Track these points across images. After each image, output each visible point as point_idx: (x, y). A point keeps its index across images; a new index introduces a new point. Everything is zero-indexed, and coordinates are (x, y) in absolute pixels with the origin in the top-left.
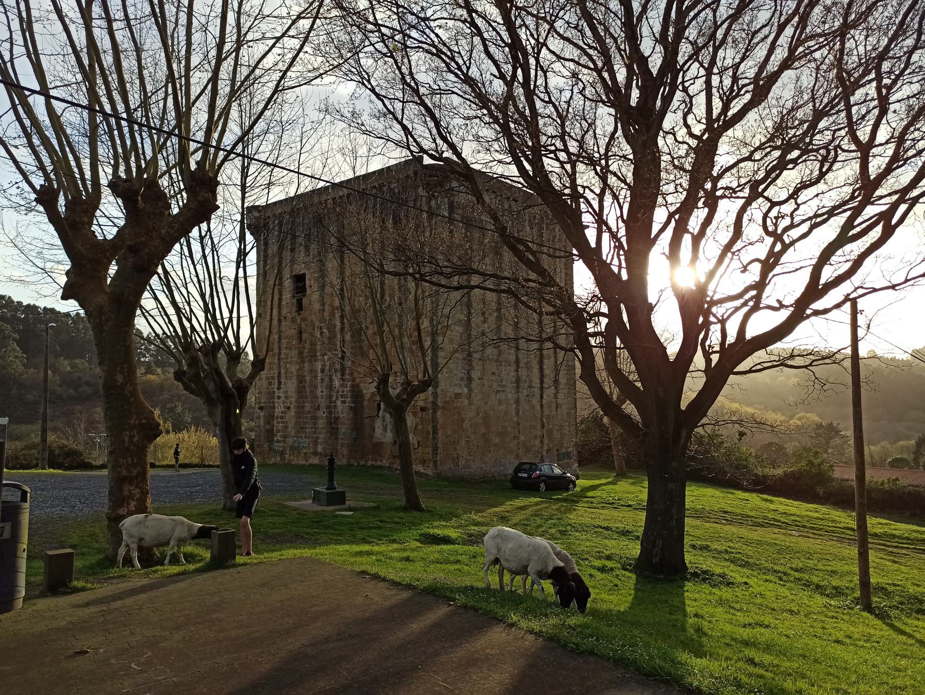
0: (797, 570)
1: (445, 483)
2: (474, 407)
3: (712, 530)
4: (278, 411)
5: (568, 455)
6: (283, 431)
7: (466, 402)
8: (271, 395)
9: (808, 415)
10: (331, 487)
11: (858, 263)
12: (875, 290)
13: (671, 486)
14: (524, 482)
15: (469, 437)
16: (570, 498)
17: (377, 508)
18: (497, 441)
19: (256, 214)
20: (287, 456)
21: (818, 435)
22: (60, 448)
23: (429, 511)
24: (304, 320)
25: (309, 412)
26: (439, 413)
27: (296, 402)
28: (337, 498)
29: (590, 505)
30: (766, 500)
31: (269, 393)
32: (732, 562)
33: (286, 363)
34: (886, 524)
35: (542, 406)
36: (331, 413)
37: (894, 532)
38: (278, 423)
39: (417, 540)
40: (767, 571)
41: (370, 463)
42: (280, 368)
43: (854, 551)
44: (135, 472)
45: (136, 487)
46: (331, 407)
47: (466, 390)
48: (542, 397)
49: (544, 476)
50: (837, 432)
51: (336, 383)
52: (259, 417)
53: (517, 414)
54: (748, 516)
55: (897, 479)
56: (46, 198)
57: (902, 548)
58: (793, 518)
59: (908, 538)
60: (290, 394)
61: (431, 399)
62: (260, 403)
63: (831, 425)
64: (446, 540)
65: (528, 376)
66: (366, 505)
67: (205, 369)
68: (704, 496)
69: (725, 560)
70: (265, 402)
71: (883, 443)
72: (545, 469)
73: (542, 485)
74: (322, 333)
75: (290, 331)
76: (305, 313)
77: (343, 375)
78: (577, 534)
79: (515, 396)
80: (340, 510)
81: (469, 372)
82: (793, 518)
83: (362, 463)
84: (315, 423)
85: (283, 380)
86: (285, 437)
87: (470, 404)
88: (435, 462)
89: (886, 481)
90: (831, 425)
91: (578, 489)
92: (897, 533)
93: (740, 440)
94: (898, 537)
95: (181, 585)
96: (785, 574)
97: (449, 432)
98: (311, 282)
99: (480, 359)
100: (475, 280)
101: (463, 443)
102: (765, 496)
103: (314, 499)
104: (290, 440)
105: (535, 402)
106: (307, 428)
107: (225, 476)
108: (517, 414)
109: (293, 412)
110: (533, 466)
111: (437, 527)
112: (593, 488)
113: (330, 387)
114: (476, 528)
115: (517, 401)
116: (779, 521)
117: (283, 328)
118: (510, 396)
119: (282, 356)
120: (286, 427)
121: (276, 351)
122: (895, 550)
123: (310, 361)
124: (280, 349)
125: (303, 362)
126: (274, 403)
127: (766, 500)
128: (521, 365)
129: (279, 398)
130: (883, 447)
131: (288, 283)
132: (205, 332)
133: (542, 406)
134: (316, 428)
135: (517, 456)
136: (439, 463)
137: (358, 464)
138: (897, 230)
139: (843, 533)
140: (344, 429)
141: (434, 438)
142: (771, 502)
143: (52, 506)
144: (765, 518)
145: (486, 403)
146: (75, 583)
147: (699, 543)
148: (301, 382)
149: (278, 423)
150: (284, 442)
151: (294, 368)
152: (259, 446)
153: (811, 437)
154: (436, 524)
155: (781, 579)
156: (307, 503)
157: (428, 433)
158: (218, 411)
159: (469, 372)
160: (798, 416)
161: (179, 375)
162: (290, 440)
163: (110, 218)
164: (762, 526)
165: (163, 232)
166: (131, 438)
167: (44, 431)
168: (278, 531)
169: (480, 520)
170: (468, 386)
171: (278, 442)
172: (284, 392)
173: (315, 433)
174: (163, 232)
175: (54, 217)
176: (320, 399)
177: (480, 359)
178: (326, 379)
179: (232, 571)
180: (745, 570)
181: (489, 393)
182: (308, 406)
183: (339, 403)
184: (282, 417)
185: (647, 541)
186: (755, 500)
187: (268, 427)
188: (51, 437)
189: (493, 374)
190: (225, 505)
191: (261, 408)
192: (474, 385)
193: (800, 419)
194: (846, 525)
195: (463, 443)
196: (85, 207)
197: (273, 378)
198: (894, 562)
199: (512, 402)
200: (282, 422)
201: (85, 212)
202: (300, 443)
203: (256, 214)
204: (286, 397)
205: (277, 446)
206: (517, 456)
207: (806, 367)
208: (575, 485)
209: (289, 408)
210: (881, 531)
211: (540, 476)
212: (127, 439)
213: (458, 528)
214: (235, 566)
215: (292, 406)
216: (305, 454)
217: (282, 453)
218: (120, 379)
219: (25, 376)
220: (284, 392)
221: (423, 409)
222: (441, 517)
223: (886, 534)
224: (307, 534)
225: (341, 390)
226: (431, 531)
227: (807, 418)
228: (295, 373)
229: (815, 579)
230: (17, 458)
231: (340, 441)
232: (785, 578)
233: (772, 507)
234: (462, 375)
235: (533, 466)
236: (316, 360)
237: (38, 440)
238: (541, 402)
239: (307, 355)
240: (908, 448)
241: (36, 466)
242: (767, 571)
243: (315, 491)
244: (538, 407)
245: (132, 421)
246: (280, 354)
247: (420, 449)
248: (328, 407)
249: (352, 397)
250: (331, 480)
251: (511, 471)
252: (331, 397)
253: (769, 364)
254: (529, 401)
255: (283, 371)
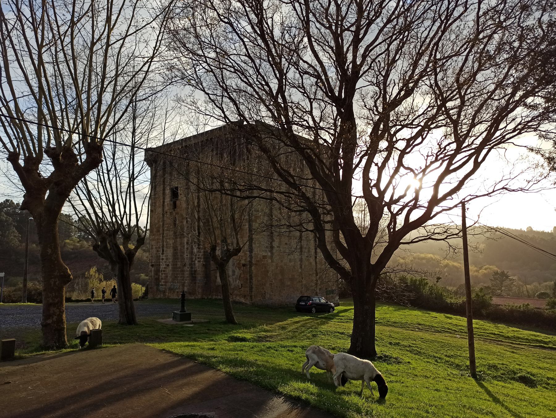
0: (449, 357)
2: (274, 264)
3: (406, 334)
4: (162, 267)
5: (332, 292)
7: (270, 261)
8: (158, 258)
9: (491, 267)
10: (183, 310)
11: (461, 183)
12: (477, 197)
13: (366, 307)
14: (303, 307)
17: (209, 322)
18: (289, 283)
20: (167, 294)
21: (496, 279)
22: (35, 290)
24: (177, 213)
25: (180, 268)
26: (253, 268)
27: (172, 262)
28: (185, 317)
30: (448, 317)
32: (411, 352)
33: (167, 239)
34: (517, 331)
35: (316, 262)
36: (192, 268)
37: (519, 336)
38: (162, 274)
41: (214, 297)
43: (466, 342)
44: (56, 301)
46: (192, 264)
47: (269, 254)
48: (316, 257)
50: (507, 277)
51: (195, 250)
53: (301, 267)
54: (433, 327)
55: (528, 305)
56: (13, 158)
57: (522, 345)
58: (460, 327)
59: (527, 339)
60: (169, 257)
61: (248, 259)
62: (152, 262)
64: (243, 340)
65: (307, 245)
67: (111, 242)
68: (410, 315)
69: (407, 350)
71: (534, 284)
72: (316, 300)
73: (314, 309)
74: (187, 222)
75: (168, 220)
76: (178, 210)
77: (199, 245)
78: (323, 336)
79: (300, 257)
80: (186, 324)
81: (271, 243)
82: (460, 327)
83: (210, 297)
84: (183, 274)
85: (165, 249)
86: (166, 282)
87: (272, 262)
88: (251, 296)
91: (335, 312)
92: (521, 336)
93: (437, 282)
94: (521, 338)
96: (440, 358)
97: (259, 279)
102: (448, 315)
103: (173, 318)
104: (169, 284)
105: (312, 260)
107: (120, 304)
108: (301, 267)
109: (170, 268)
110: (309, 298)
111: (240, 333)
112: (345, 311)
113: (192, 253)
114: (264, 333)
115: (301, 260)
116: (451, 329)
117: (165, 219)
118: (296, 257)
119: (165, 235)
120: (167, 277)
122: (516, 346)
123: (180, 238)
124: (163, 230)
125: (176, 238)
126: (160, 262)
127: (448, 317)
128: (303, 238)
129: (163, 259)
130: (535, 286)
131: (168, 191)
132: (122, 219)
133: (316, 262)
134: (184, 277)
135: (301, 292)
137: (208, 298)
138: (482, 165)
139: (488, 336)
141: (250, 282)
142: (451, 318)
143: (24, 323)
145: (282, 261)
146: (16, 354)
147: (394, 341)
149: (162, 274)
150: (166, 285)
151: (171, 242)
152: (151, 288)
153: (492, 280)
154: (241, 331)
155: (436, 361)
156: (170, 321)
157: (247, 279)
158: (117, 268)
159: (271, 243)
160: (485, 267)
161: (95, 247)
162: (169, 284)
164: (440, 332)
165: (73, 174)
166: (55, 282)
167: (25, 280)
168: (147, 335)
169: (269, 329)
171: (162, 285)
172: (166, 256)
173: (183, 280)
174: (73, 174)
175: (17, 167)
176: (186, 260)
180: (417, 356)
181: (288, 255)
182: (179, 264)
183: (196, 262)
184: (164, 271)
185: (354, 337)
187: (156, 277)
188: (30, 285)
189: (286, 244)
190: (120, 321)
191: (152, 266)
192: (274, 251)
193: (486, 269)
194: (491, 332)
197: (159, 248)
199: (298, 260)
200: (164, 274)
202: (174, 286)
203: (151, 153)
204: (167, 259)
206: (301, 292)
207: (443, 239)
208: (334, 310)
209: (168, 265)
210: (512, 335)
211: (312, 304)
212: (52, 283)
213: (253, 333)
214: (101, 348)
216: (178, 292)
217: (164, 292)
218: (49, 251)
219: (20, 247)
220: (166, 256)
221: (244, 265)
223: (514, 337)
224: (163, 336)
225: (198, 254)
226: (236, 335)
227: (490, 269)
228: (172, 245)
229: (457, 361)
230: (10, 296)
232: (439, 361)
233: (450, 321)
234: (267, 245)
235: (309, 298)
236: (184, 237)
237: (21, 286)
239: (179, 235)
240: (550, 286)
241: (20, 301)
243: (174, 313)
244: (314, 263)
245: (56, 274)
246: (163, 234)
247: (243, 289)
248: (191, 264)
249: (204, 258)
250: (183, 306)
251: (295, 302)
252: (192, 258)
253: (423, 238)
254: (308, 260)
255: (165, 243)
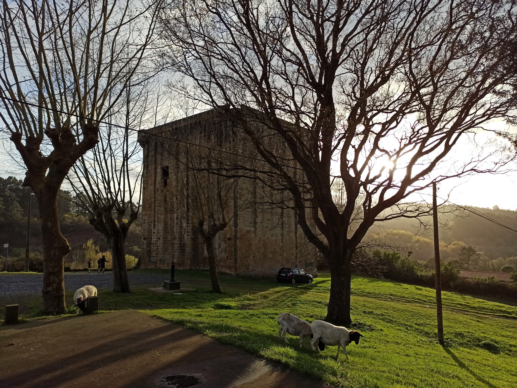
1: (240, 279)
2: (257, 238)
4: (154, 240)
5: (311, 264)
6: (156, 251)
7: (253, 235)
8: (150, 231)
9: (459, 242)
10: (172, 280)
12: (447, 177)
14: (284, 278)
15: (255, 254)
16: (308, 287)
17: (197, 291)
18: (271, 256)
19: (143, 134)
20: (158, 265)
21: (463, 254)
23: (225, 293)
24: (167, 191)
25: (170, 241)
26: (238, 241)
27: (163, 235)
28: (175, 286)
29: (318, 291)
30: (418, 289)
31: (149, 230)
32: (383, 320)
33: (158, 214)
34: (482, 302)
35: (296, 237)
37: (484, 306)
38: (154, 246)
39: (212, 307)
40: (400, 324)
41: (201, 268)
42: (155, 217)
43: (435, 312)
45: (57, 277)
46: (181, 238)
47: (253, 229)
48: (296, 233)
49: (295, 275)
50: (474, 252)
51: (184, 225)
52: (143, 244)
53: (282, 241)
54: (404, 297)
55: (493, 278)
56: (16, 138)
58: (429, 298)
59: (492, 309)
60: (160, 231)
62: (144, 236)
63: (470, 248)
64: (228, 307)
66: (191, 289)
67: (106, 217)
70: (147, 235)
71: (500, 258)
72: (296, 271)
74: (177, 199)
77: (188, 220)
78: (302, 305)
81: (255, 219)
82: (429, 298)
83: (197, 268)
84: (173, 247)
85: (156, 224)
86: (157, 254)
87: (255, 236)
88: (236, 268)
89: (487, 279)
90: (470, 248)
92: (486, 307)
93: (409, 256)
94: (486, 309)
95: (69, 321)
98: (171, 171)
99: (261, 212)
100: (241, 172)
101: (251, 258)
102: (418, 287)
103: (164, 287)
104: (160, 256)
105: (292, 235)
106: (169, 249)
108: (282, 241)
109: (161, 241)
110: (289, 270)
113: (181, 227)
114: (248, 302)
115: (282, 235)
116: (421, 300)
117: (157, 195)
118: (278, 232)
119: (156, 210)
120: (158, 249)
121: (153, 208)
123: (171, 213)
124: (155, 206)
125: (167, 214)
126: (151, 236)
127: (418, 289)
128: (285, 215)
129: (154, 233)
131: (159, 170)
133: (296, 237)
134: (173, 249)
136: (238, 268)
138: (452, 147)
139: (455, 306)
140: (188, 250)
141: (235, 255)
143: (26, 290)
144: (413, 298)
145: (264, 236)
146: (20, 318)
147: (368, 310)
148: (166, 224)
149: (154, 246)
150: (157, 257)
151: (162, 217)
152: (143, 259)
153: (459, 255)
155: (407, 329)
156: (160, 289)
157: (232, 252)
158: (112, 241)
159: (255, 219)
161: (92, 221)
162: (160, 256)
163: (47, 148)
164: (411, 302)
165: (71, 153)
167: (27, 251)
170: (254, 227)
171: (154, 257)
174: (71, 153)
175: (19, 147)
176: (176, 233)
177: (261, 212)
178: (179, 223)
179: (95, 316)
180: (389, 324)
181: (269, 230)
182: (169, 237)
183: (185, 236)
184: (155, 244)
185: (331, 306)
186: (411, 288)
187: (148, 249)
188: (32, 255)
189: (269, 220)
191: (145, 239)
192: (257, 226)
193: (454, 245)
194: (458, 302)
195: (251, 258)
196: (34, 142)
197: (151, 222)
198: (478, 321)
201: (35, 144)
203: (143, 134)
204: (158, 233)
205: (153, 259)
207: (415, 217)
208: (312, 281)
209: (159, 239)
210: (478, 305)
211: (292, 275)
212: (52, 254)
215: (161, 238)
216: (168, 263)
217: (155, 263)
218: (50, 224)
219: (23, 221)
221: (229, 239)
222: (231, 296)
223: (480, 307)
225: (186, 229)
226: (221, 303)
227: (458, 244)
229: (426, 329)
231: (186, 256)
232: (409, 328)
233: (420, 292)
235: (289, 270)
236: (174, 213)
237: (24, 256)
238: (296, 235)
239: (169, 210)
241: (23, 270)
242: (400, 324)
243: (164, 282)
244: (294, 238)
245: (55, 245)
246: (155, 209)
248: (180, 238)
250: (173, 276)
252: (181, 232)
253: (396, 215)
254: (289, 235)
